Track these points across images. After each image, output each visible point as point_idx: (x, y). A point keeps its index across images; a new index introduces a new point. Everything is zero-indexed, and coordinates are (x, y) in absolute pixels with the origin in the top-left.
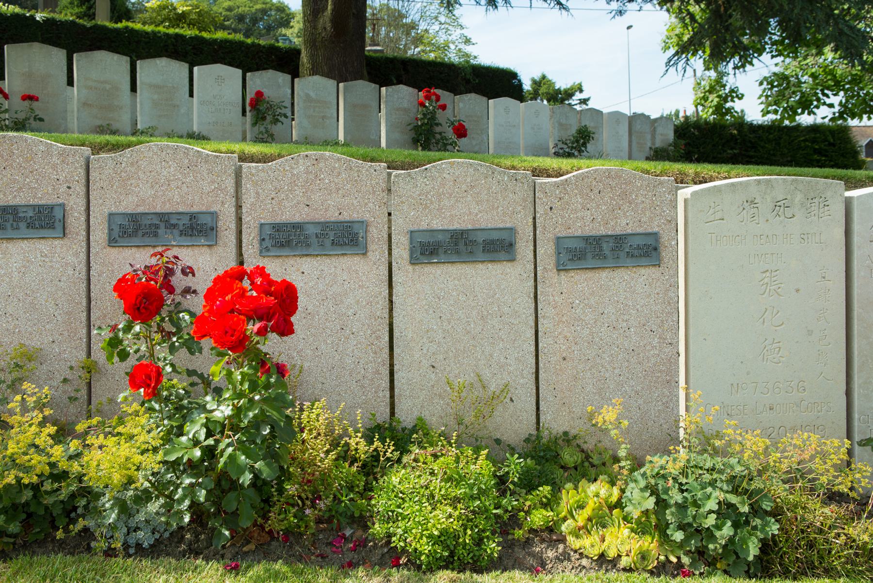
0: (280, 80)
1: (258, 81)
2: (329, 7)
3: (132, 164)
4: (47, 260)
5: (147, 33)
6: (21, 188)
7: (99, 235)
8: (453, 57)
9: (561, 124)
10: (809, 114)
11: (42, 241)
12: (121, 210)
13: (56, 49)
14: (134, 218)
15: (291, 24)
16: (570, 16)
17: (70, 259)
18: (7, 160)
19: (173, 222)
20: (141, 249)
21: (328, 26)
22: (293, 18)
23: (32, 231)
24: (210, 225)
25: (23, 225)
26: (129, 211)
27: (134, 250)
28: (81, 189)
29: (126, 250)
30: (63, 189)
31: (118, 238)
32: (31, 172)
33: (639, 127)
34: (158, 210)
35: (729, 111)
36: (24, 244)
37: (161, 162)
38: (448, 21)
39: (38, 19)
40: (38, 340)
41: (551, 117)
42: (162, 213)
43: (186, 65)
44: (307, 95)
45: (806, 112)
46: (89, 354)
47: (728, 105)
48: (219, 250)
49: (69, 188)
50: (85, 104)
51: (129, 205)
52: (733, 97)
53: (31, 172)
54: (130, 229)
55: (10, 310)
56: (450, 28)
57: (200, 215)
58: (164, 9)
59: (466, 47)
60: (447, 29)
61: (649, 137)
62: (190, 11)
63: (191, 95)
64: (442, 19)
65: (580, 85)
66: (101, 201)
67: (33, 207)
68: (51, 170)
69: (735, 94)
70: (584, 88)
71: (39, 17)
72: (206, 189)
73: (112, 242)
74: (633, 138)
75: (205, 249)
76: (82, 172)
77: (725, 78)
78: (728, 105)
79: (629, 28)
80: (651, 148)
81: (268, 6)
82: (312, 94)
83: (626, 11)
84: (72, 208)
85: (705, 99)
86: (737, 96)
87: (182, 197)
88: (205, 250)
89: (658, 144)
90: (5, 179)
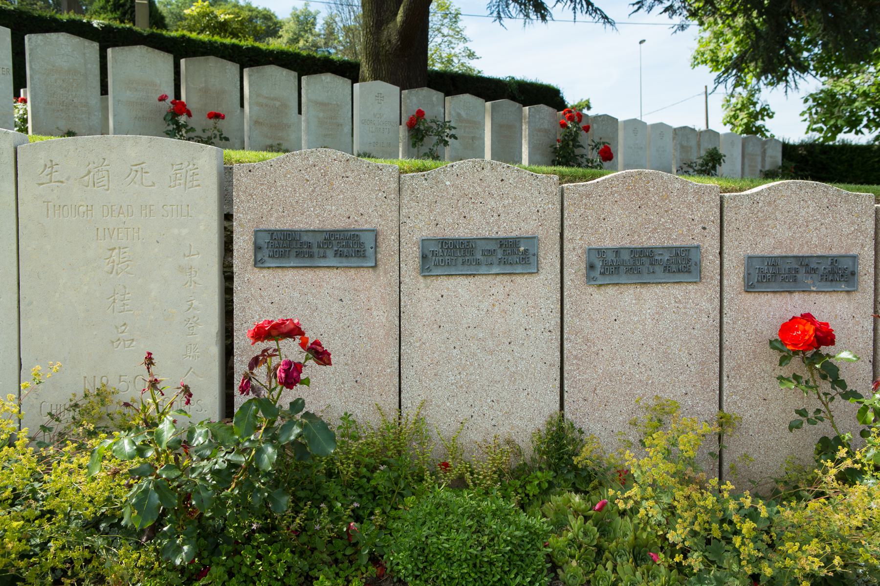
0: (434, 99)
1: (414, 100)
2: (399, 18)
3: (769, 204)
4: (681, 306)
5: (204, 43)
6: (656, 229)
7: (734, 279)
8: (456, 68)
9: (682, 147)
10: (857, 133)
11: (677, 286)
12: (758, 252)
13: (230, 63)
14: (774, 262)
15: (280, 33)
16: (615, 31)
17: (705, 305)
18: (643, 198)
19: (813, 265)
20: (778, 295)
21: (394, 38)
22: (281, 27)
23: (668, 275)
24: (851, 269)
25: (657, 268)
26: (766, 253)
27: (770, 295)
28: (715, 230)
29: (762, 295)
30: (698, 229)
31: (755, 284)
32: (666, 211)
33: (751, 149)
34: (796, 252)
35: (759, 130)
36: (658, 289)
37: (799, 201)
38: (451, 33)
39: (95, 25)
40: (671, 392)
41: (674, 138)
42: (803, 257)
43: (349, 82)
44: (459, 115)
45: (854, 131)
46: (720, 407)
47: (759, 123)
48: (858, 296)
49: (704, 228)
50: (256, 123)
51: (766, 247)
52: (763, 116)
53: (666, 211)
54: (772, 273)
55: (643, 360)
56: (453, 40)
57: (842, 259)
58: (204, 16)
59: (470, 61)
60: (451, 42)
61: (759, 159)
62: (233, 20)
63: (300, 112)
64: (445, 31)
65: (588, 101)
66: (737, 243)
67: (669, 249)
68: (686, 209)
69: (765, 112)
70: (592, 105)
71: (95, 23)
72: (846, 231)
73: (749, 288)
74: (746, 160)
75: (843, 295)
76: (718, 211)
77: (756, 96)
78: (759, 123)
79: (641, 42)
80: (761, 171)
81: (255, 13)
82: (463, 113)
83: (688, 25)
84: (707, 250)
85: (735, 117)
86: (768, 115)
87: (820, 239)
88: (843, 296)
89: (767, 167)
90: (640, 219)
